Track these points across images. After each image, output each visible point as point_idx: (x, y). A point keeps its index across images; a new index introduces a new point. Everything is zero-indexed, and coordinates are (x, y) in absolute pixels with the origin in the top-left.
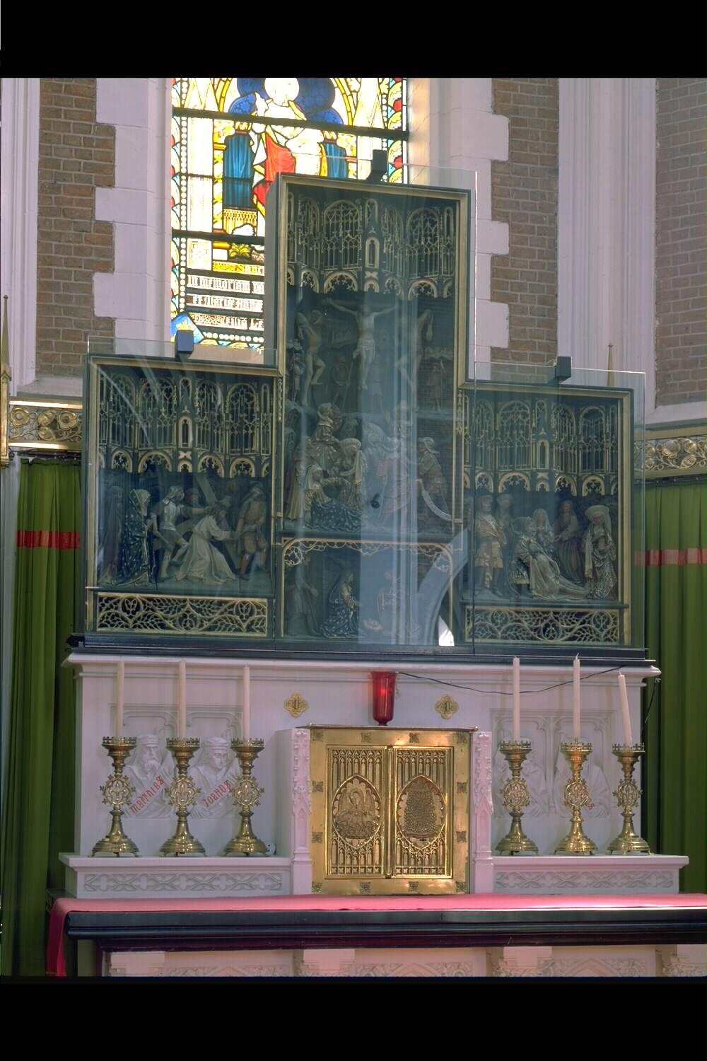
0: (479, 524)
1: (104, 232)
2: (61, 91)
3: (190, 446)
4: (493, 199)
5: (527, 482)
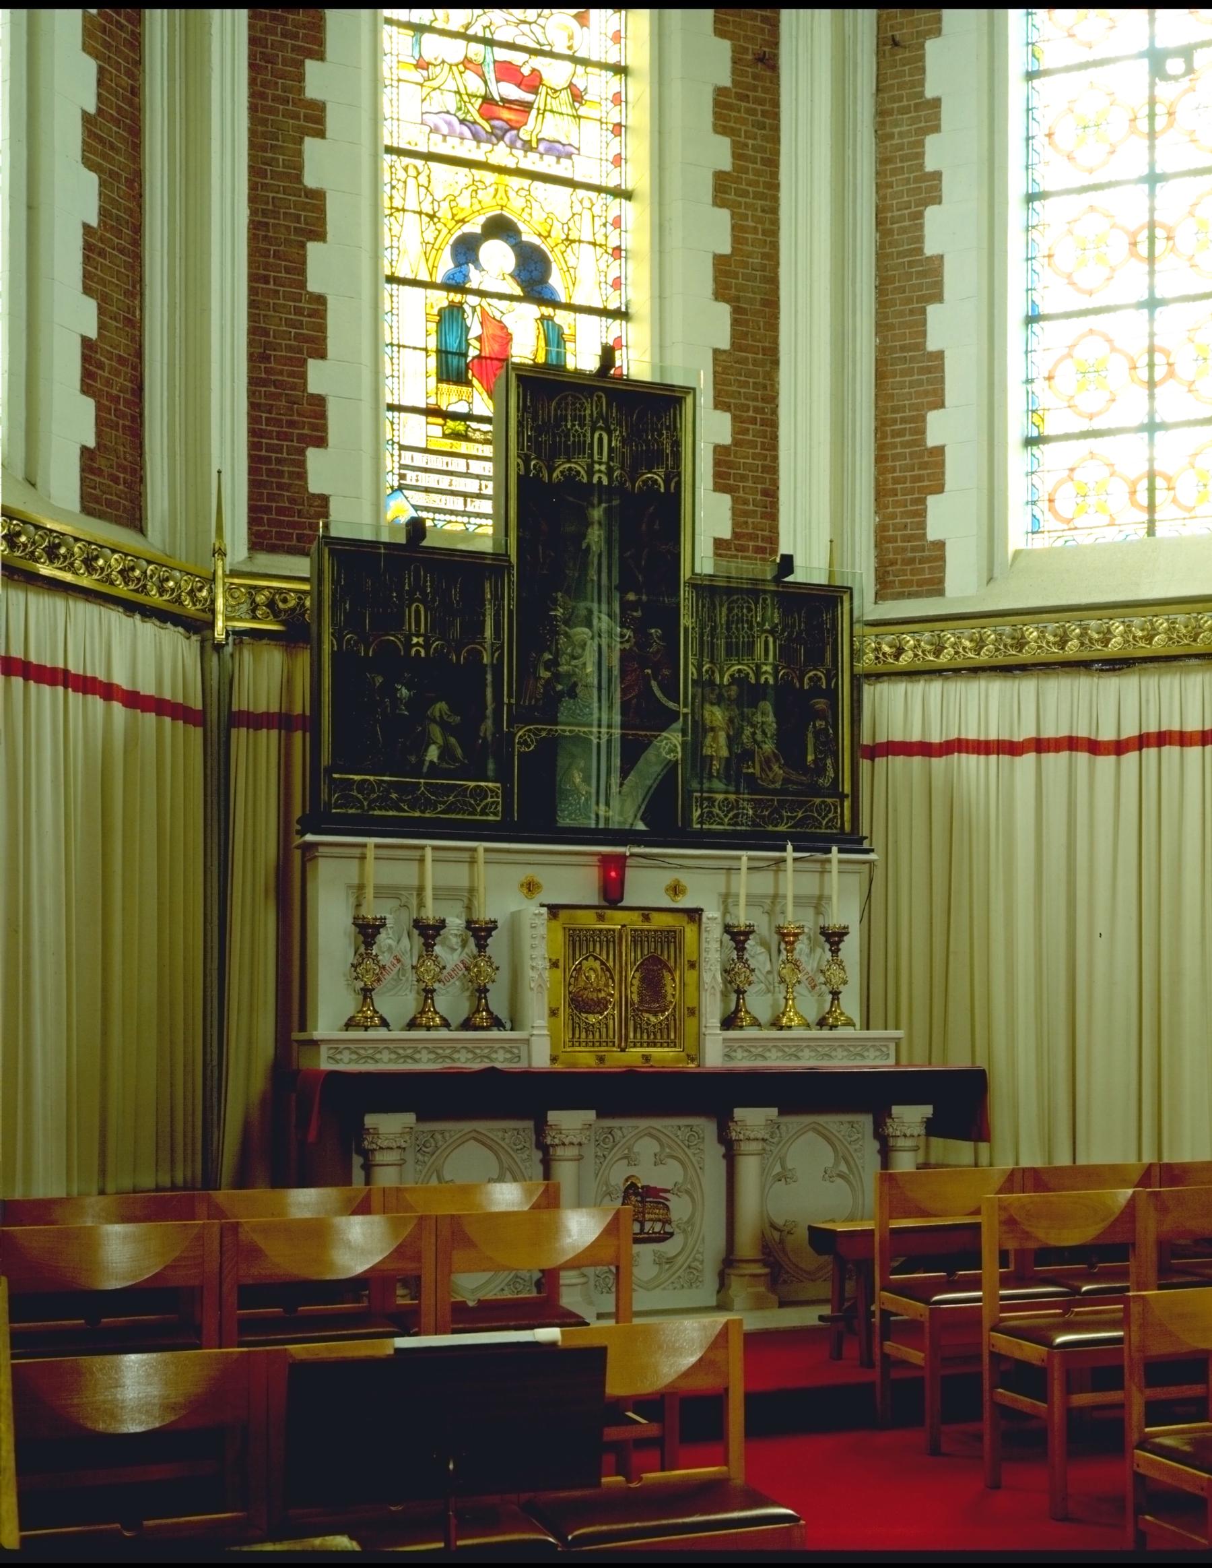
0: (707, 714)
1: (318, 405)
2: (269, 257)
3: (422, 631)
4: (715, 388)
5: (752, 675)
